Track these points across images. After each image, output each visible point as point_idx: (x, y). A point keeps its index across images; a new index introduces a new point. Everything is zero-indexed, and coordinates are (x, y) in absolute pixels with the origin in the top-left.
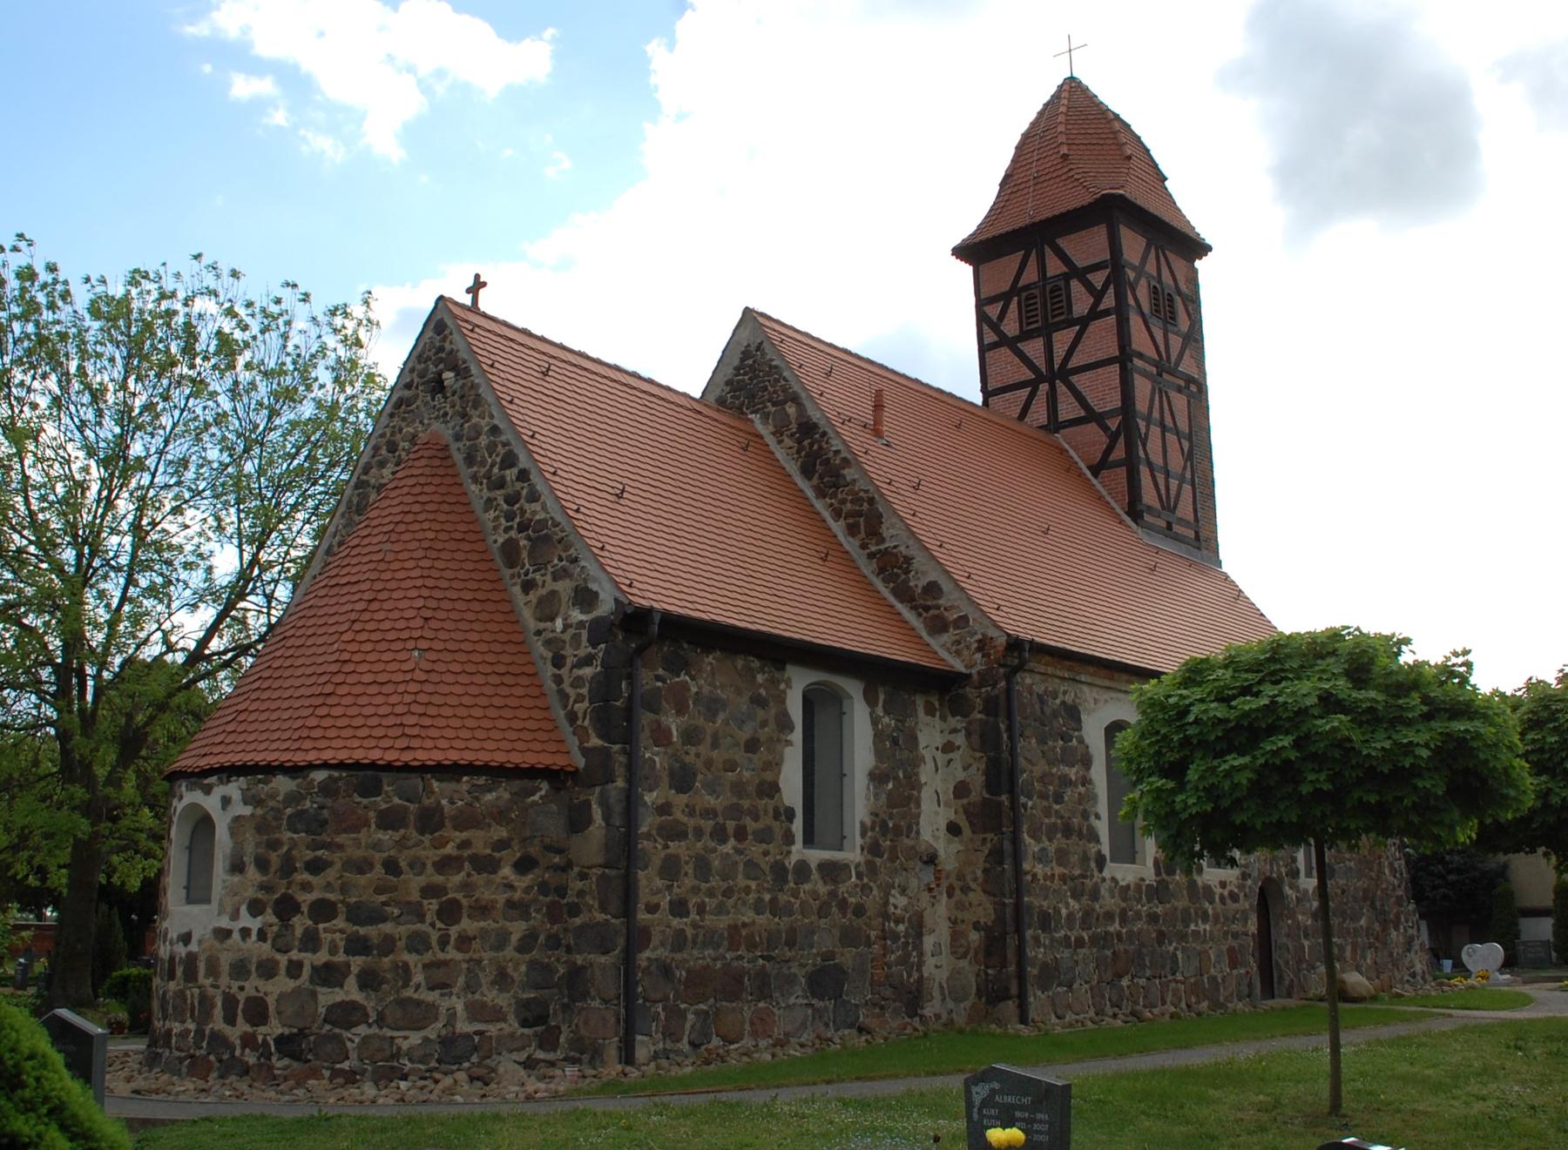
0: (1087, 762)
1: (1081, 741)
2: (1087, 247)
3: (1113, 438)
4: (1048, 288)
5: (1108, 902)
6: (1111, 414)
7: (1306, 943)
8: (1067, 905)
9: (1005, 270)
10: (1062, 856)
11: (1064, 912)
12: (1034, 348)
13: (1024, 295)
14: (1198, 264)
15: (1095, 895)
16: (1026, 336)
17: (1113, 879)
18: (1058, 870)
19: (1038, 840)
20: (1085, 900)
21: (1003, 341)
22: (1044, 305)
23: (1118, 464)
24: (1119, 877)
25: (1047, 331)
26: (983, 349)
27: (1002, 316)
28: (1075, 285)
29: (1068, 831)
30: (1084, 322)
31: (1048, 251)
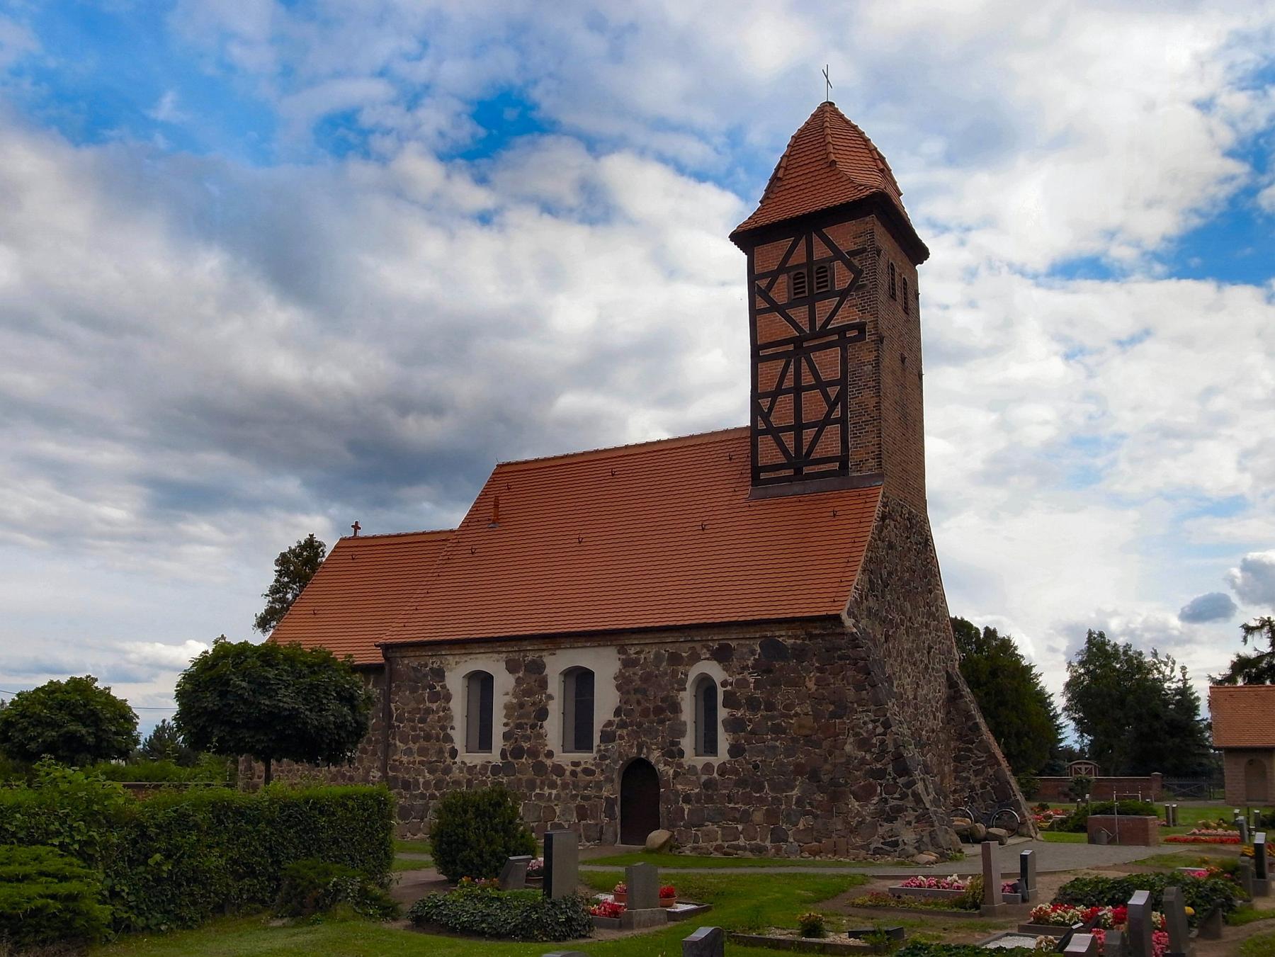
0: (448, 698)
1: (444, 687)
2: (845, 236)
3: (832, 406)
4: (815, 268)
5: (456, 773)
6: (832, 383)
7: (686, 807)
8: (424, 777)
9: (773, 254)
10: (422, 751)
11: (421, 780)
12: (800, 315)
13: (792, 273)
14: (918, 267)
15: (447, 770)
16: (793, 304)
17: (463, 762)
18: (418, 759)
19: (406, 743)
20: (439, 774)
21: (774, 307)
22: (810, 283)
23: (836, 421)
24: (467, 761)
25: (811, 301)
26: (754, 313)
27: (770, 286)
28: (838, 264)
29: (428, 738)
30: (844, 294)
31: (815, 237)
